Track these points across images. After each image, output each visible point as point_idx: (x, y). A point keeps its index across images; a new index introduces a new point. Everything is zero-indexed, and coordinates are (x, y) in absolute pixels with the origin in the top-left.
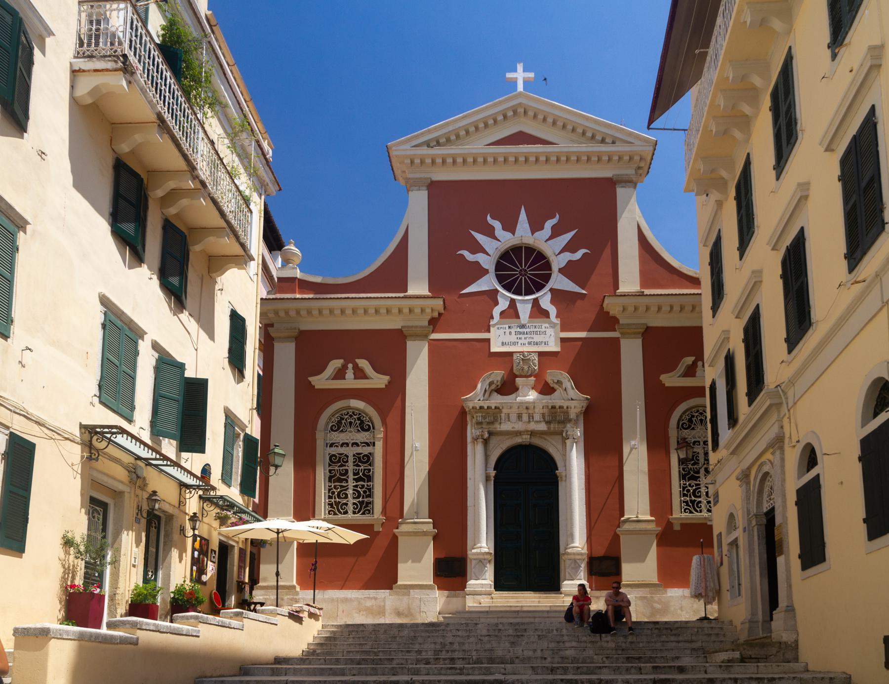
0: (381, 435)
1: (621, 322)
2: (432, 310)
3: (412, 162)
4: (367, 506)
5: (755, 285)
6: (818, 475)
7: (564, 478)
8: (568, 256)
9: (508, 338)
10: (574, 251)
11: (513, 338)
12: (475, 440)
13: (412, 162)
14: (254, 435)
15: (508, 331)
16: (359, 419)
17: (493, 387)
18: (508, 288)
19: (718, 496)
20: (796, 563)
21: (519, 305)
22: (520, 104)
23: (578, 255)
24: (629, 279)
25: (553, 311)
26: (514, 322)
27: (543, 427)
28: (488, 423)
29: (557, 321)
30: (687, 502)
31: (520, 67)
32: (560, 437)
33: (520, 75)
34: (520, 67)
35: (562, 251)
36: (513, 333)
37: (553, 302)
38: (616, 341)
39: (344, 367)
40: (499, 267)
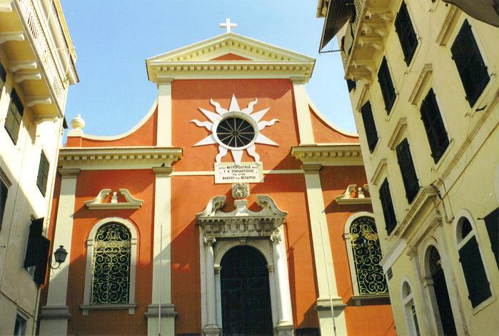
0: (136, 241)
1: (304, 163)
2: (174, 157)
3: (162, 69)
4: (123, 295)
5: (402, 127)
6: (474, 237)
7: (272, 270)
8: (265, 123)
9: (227, 175)
10: (269, 120)
11: (230, 175)
12: (205, 245)
13: (162, 69)
14: (47, 237)
15: (227, 170)
16: (119, 231)
17: (218, 207)
18: (226, 142)
19: (391, 272)
20: (467, 303)
21: (233, 152)
22: (229, 39)
23: (272, 122)
24: (307, 138)
25: (257, 157)
26: (231, 164)
27: (255, 234)
28: (215, 232)
29: (261, 163)
30: (363, 285)
31: (228, 20)
32: (268, 241)
33: (229, 24)
34: (228, 20)
35: (261, 120)
36: (231, 171)
37: (257, 151)
38: (302, 175)
39: (111, 194)
40: (219, 130)
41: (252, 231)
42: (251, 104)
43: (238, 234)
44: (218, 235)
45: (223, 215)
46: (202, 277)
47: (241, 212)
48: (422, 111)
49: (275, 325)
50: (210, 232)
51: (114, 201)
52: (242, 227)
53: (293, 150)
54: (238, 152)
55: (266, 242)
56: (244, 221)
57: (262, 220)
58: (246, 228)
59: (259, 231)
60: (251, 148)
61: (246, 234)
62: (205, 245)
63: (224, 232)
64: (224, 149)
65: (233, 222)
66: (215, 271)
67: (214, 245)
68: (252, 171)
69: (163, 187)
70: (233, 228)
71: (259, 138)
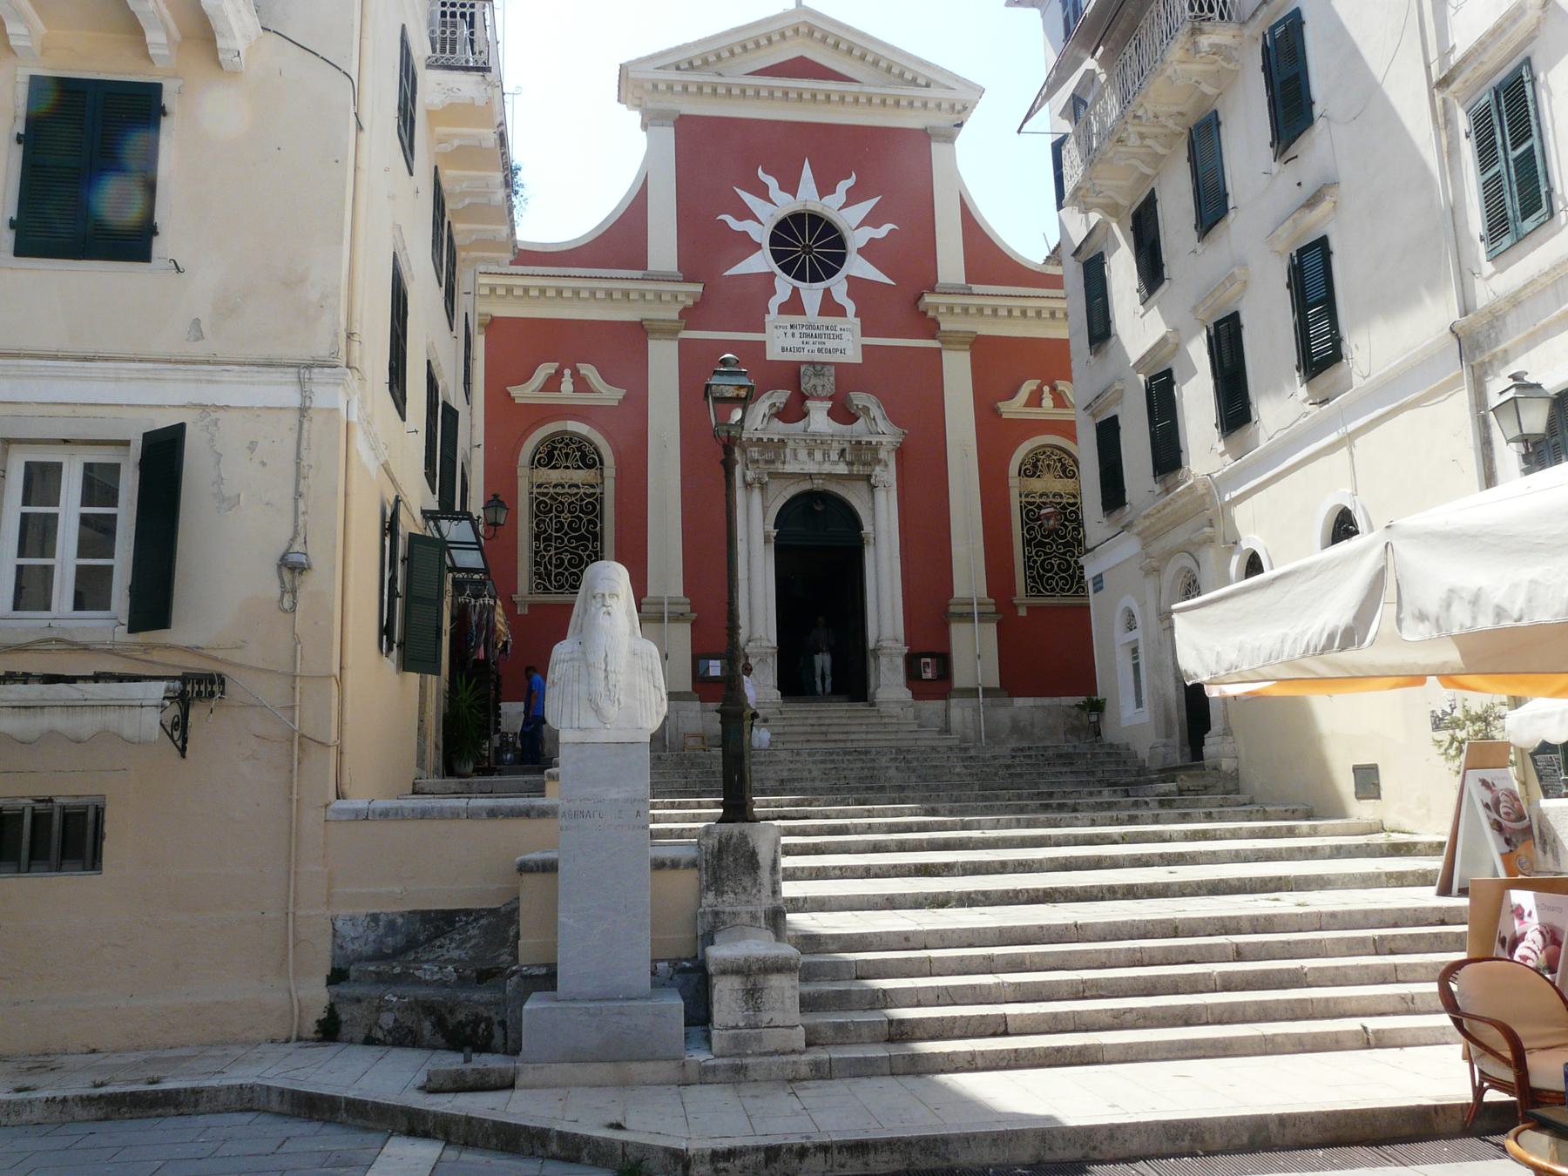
8: (868, 233)
9: (790, 342)
15: (789, 331)
16: (579, 449)
25: (850, 307)
27: (842, 469)
28: (767, 462)
38: (939, 351)
40: (774, 240)
41: (835, 463)
42: (844, 186)
43: (812, 468)
44: (772, 468)
46: (741, 547)
52: (818, 455)
54: (811, 294)
55: (862, 487)
59: (850, 464)
60: (838, 286)
64: (784, 285)
67: (763, 487)
68: (839, 337)
69: (663, 360)
71: (857, 266)
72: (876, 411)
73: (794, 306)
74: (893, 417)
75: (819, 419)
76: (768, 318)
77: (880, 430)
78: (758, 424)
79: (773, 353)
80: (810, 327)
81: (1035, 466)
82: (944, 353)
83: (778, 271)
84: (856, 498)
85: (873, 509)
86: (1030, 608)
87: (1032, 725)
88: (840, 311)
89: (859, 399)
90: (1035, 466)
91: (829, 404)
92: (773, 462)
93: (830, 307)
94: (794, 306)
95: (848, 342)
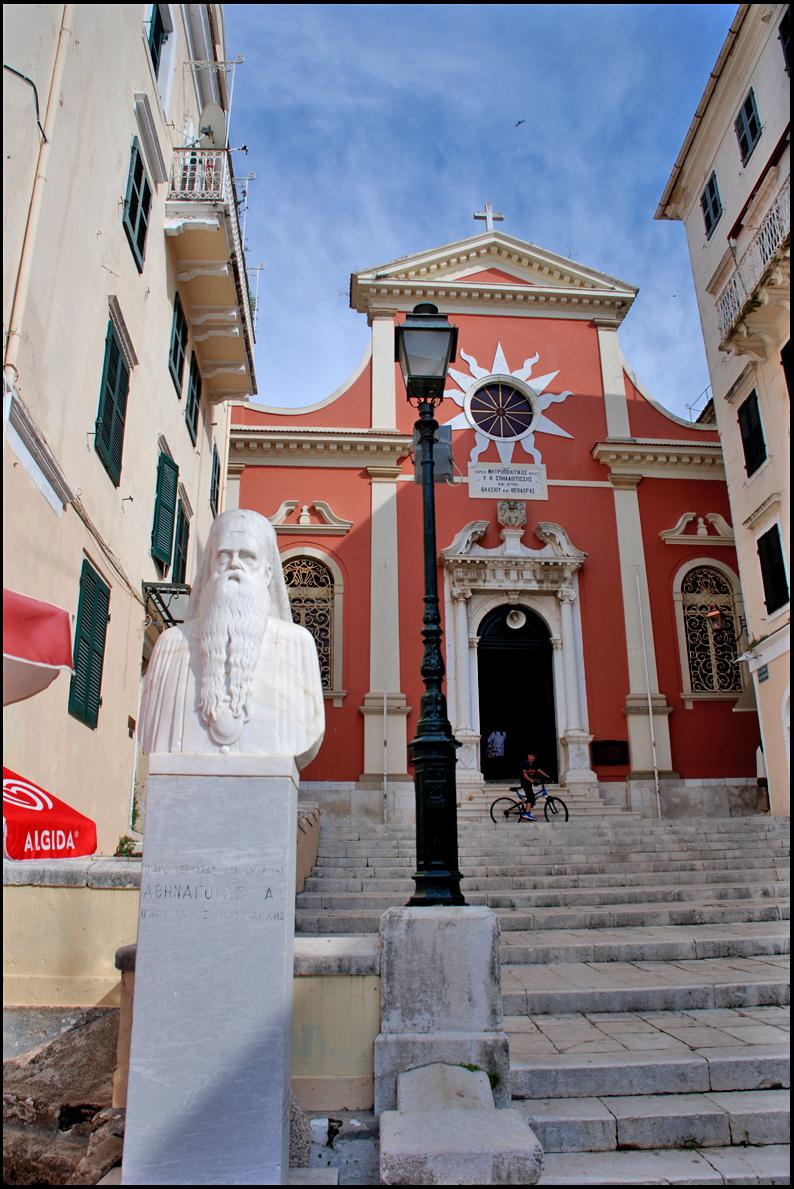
9: (488, 484)
11: (494, 484)
15: (488, 475)
17: (476, 537)
25: (537, 456)
27: (534, 586)
28: (471, 580)
29: (544, 466)
36: (494, 478)
38: (610, 491)
42: (529, 363)
43: (507, 585)
44: (475, 586)
45: (480, 553)
47: (513, 546)
48: (741, 412)
49: (561, 734)
50: (462, 580)
51: (702, 531)
52: (513, 575)
53: (600, 448)
54: (506, 446)
55: (551, 600)
56: (512, 565)
57: (547, 564)
58: (520, 573)
59: (540, 582)
60: (527, 439)
61: (521, 586)
62: (454, 600)
63: (485, 581)
64: (483, 439)
65: (527, 565)
66: (470, 643)
67: (467, 601)
68: (530, 479)
70: (500, 574)
71: (541, 423)
72: (561, 538)
73: (491, 455)
74: (575, 541)
75: (513, 546)
76: (470, 464)
77: (563, 550)
78: (463, 549)
79: (475, 493)
80: (505, 471)
81: (695, 583)
82: (617, 494)
83: (478, 428)
84: (545, 610)
85: (560, 619)
86: (696, 703)
87: (701, 803)
88: (530, 459)
89: (549, 528)
90: (695, 583)
91: (521, 532)
92: (475, 580)
93: (520, 456)
94: (491, 455)
95: (536, 484)
